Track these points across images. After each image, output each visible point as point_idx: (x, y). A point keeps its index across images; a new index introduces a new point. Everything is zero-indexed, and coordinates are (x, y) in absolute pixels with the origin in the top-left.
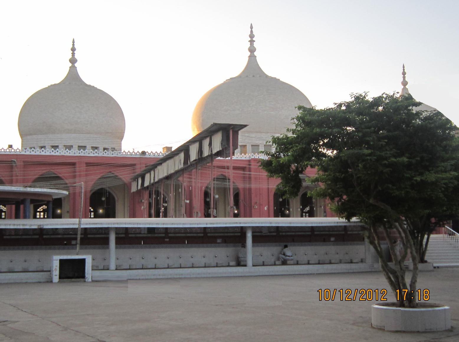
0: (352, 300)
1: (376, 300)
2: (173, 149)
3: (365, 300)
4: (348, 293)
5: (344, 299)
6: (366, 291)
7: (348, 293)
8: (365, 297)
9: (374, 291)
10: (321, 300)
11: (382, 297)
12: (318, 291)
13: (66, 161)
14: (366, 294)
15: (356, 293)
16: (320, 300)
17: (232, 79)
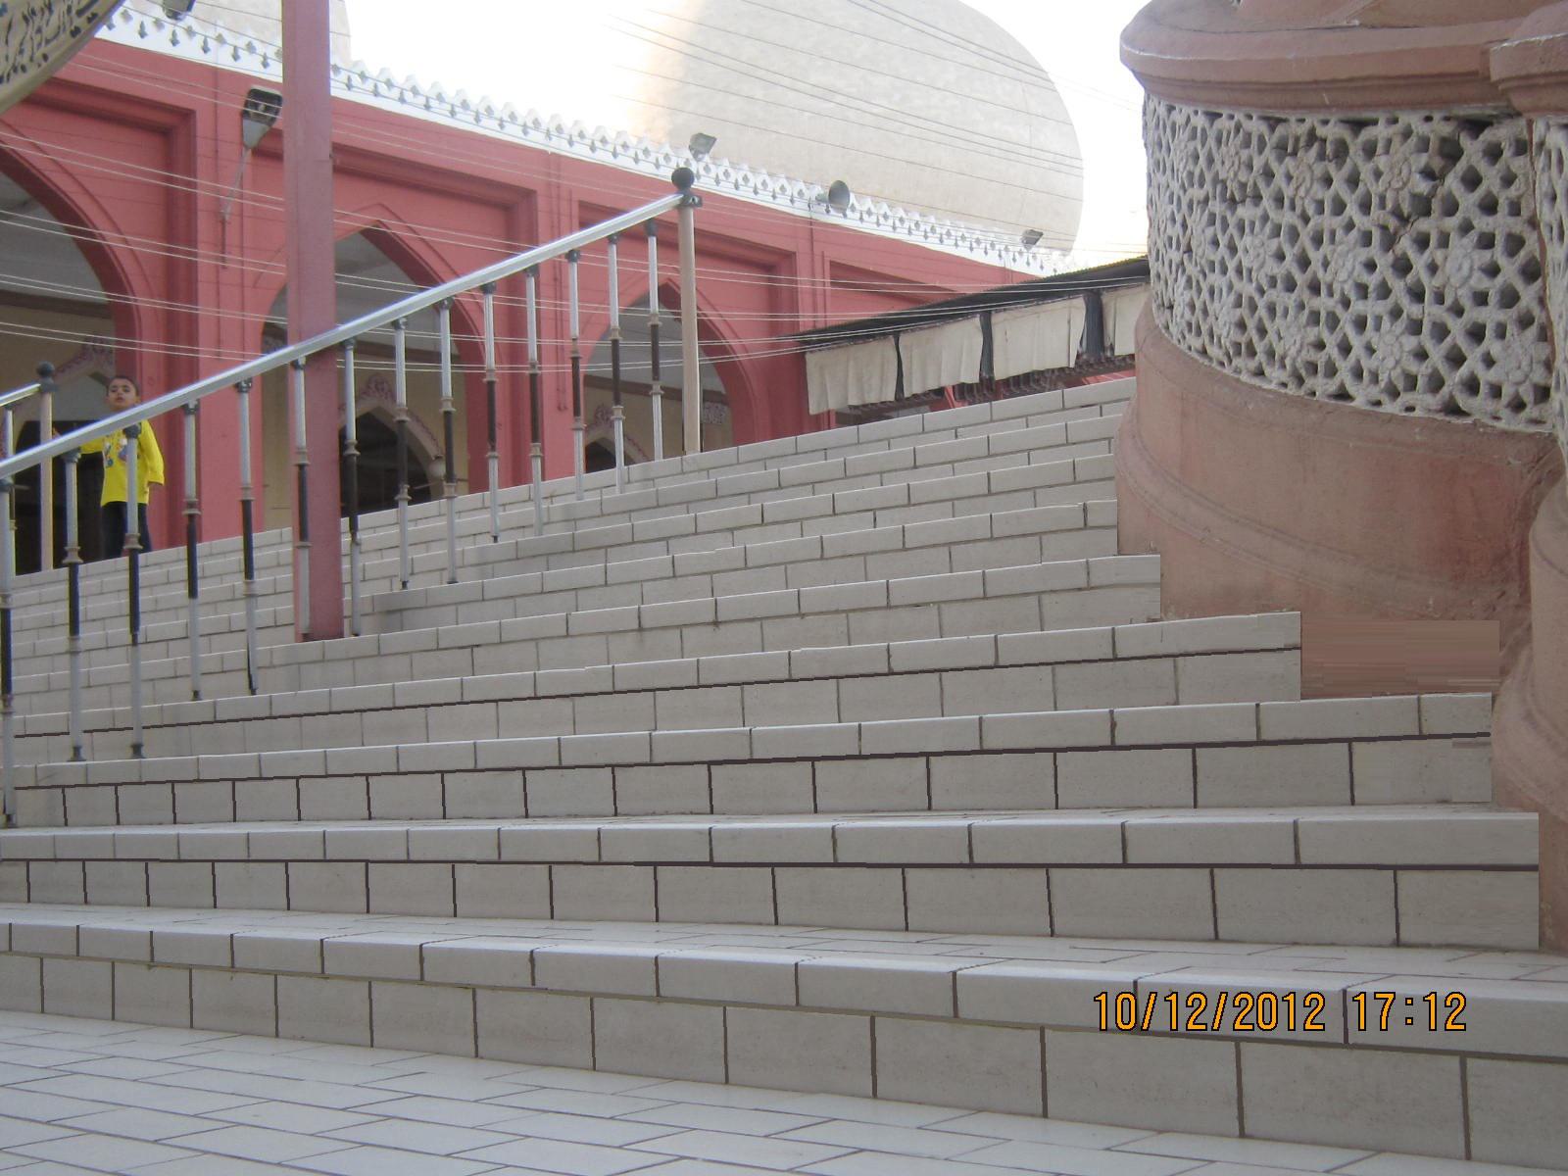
0: (1209, 1028)
1: (1430, 1030)
2: (105, 27)
3: (1251, 1027)
4: (1454, 1006)
5: (1182, 1029)
6: (1256, 998)
7: (1313, 1005)
8: (1251, 1018)
9: (1283, 1000)
10: (1294, 1030)
11: (1192, 1020)
12: (1165, 1000)
13: (770, 243)
14: (1255, 1007)
15: (1221, 1005)
16: (1360, 1030)
17: (1140, 12)
